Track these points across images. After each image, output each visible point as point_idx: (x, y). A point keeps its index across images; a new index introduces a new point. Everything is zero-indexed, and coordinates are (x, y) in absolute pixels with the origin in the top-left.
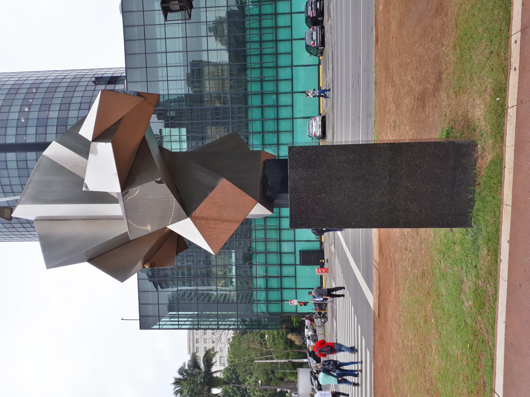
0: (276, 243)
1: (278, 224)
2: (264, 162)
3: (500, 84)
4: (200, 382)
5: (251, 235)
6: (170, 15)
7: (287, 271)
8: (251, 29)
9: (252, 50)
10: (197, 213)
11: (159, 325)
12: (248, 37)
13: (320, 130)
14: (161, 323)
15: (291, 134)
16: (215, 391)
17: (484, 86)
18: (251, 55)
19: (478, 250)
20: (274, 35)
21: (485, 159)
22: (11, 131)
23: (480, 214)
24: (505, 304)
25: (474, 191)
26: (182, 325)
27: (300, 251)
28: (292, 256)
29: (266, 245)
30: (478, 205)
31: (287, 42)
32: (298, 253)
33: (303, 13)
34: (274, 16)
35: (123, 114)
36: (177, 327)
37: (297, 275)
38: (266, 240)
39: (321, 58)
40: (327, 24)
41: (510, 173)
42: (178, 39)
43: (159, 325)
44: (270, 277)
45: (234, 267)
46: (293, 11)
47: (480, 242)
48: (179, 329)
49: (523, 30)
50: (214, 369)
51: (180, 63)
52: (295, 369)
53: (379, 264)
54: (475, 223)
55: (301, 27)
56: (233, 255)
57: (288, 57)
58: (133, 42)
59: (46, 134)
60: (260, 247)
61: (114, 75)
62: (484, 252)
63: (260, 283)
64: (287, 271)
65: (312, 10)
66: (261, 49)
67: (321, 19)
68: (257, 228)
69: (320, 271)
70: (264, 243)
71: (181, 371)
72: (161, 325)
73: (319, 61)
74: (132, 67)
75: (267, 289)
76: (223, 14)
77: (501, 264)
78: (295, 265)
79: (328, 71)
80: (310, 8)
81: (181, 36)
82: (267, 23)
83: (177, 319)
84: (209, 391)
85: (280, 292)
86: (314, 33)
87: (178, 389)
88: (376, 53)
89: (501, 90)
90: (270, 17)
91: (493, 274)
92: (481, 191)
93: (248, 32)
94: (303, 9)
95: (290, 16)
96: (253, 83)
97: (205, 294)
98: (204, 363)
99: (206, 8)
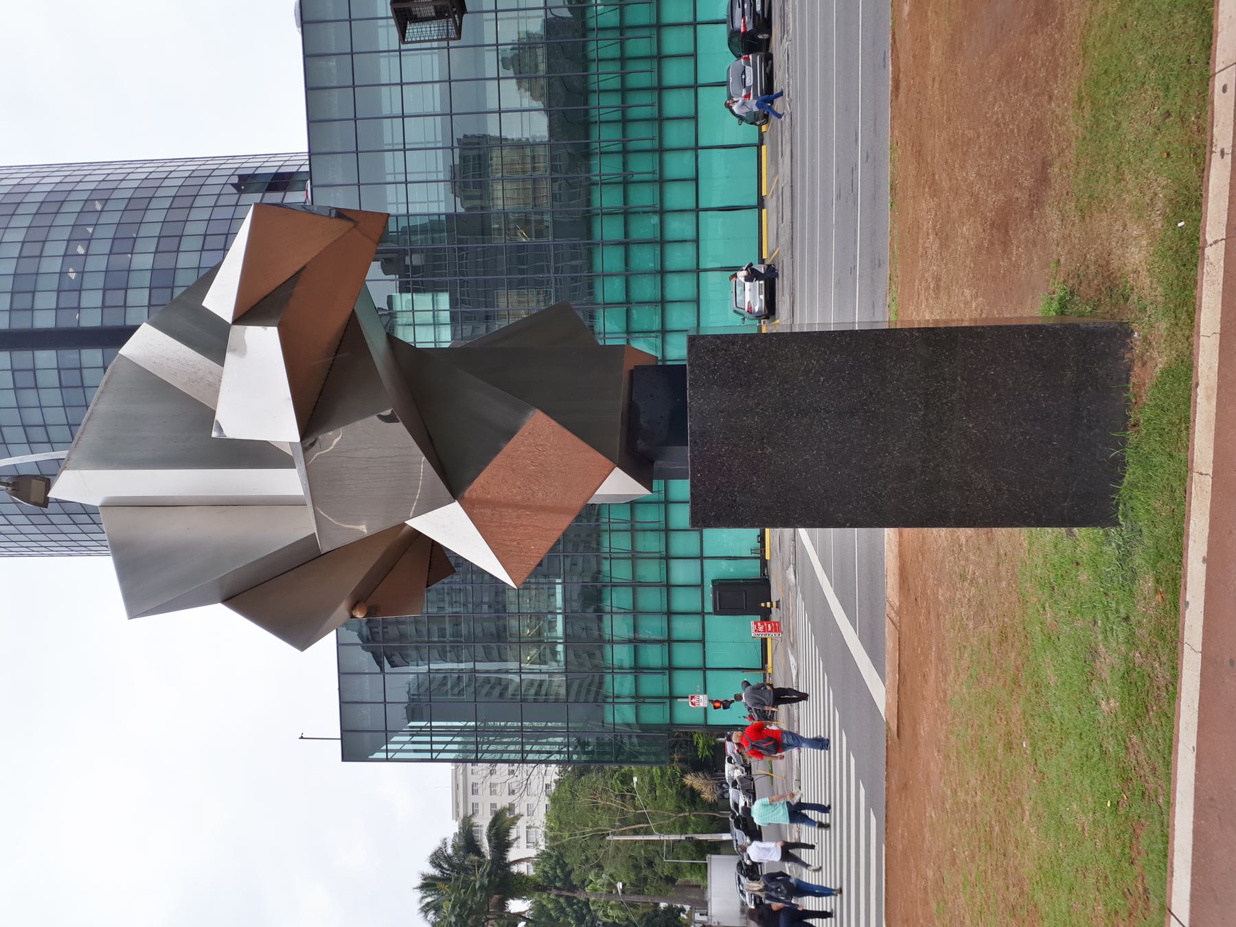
1: (662, 518)
4: (482, 886)
5: (599, 543)
6: (413, 30)
7: (684, 627)
8: (600, 60)
9: (602, 111)
11: (387, 751)
13: (762, 297)
14: (390, 747)
15: (693, 307)
16: (517, 906)
17: (1149, 194)
18: (601, 122)
19: (1133, 581)
20: (655, 40)
21: (1150, 365)
23: (1138, 497)
26: (439, 751)
27: (713, 581)
32: (709, 587)
34: (654, 31)
36: (428, 756)
37: (708, 637)
38: (634, 556)
39: (764, 128)
40: (779, 49)
42: (430, 86)
43: (387, 751)
44: (645, 641)
47: (1138, 560)
48: (432, 760)
50: (512, 855)
51: (436, 142)
52: (702, 855)
54: (1125, 516)
55: (718, 58)
56: (559, 589)
57: (688, 126)
58: (326, 93)
60: (621, 571)
61: (282, 170)
62: (1146, 584)
63: (621, 655)
64: (684, 627)
65: (743, 16)
66: (624, 108)
67: (766, 36)
68: (614, 526)
69: (761, 628)
71: (437, 858)
72: (392, 751)
73: (761, 135)
74: (324, 150)
75: (638, 669)
76: (535, 25)
78: (702, 613)
79: (780, 160)
82: (640, 46)
83: (428, 739)
84: (502, 905)
85: (666, 677)
86: (749, 70)
87: (429, 899)
88: (893, 118)
90: (645, 32)
93: (593, 68)
94: (723, 14)
95: (692, 92)
97: (493, 681)
98: (490, 841)
99: (496, 11)
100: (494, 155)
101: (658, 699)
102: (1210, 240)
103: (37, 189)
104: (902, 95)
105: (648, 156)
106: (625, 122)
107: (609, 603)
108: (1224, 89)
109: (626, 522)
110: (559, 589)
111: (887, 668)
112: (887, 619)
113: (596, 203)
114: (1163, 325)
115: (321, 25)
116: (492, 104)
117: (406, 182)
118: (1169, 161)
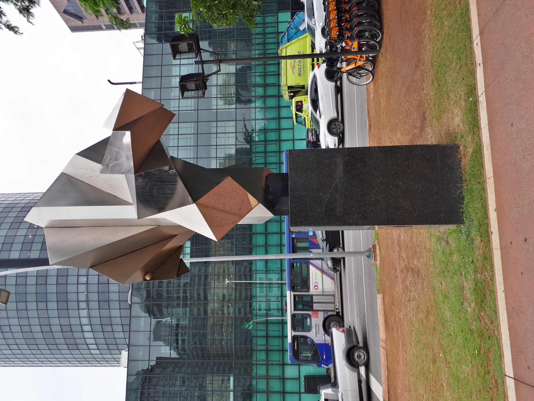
0: (279, 380)
1: (277, 70)
2: (267, 177)
3: (471, 86)
5: (251, 371)
6: (186, 94)
8: (256, 152)
10: (203, 200)
12: (254, 159)
15: (298, 381)
17: (458, 96)
18: (257, 233)
19: (473, 243)
20: (278, 157)
21: (467, 150)
22: (17, 247)
23: (470, 208)
24: (501, 272)
25: (462, 187)
27: (305, 377)
28: (296, 383)
29: (267, 355)
30: (467, 198)
31: (290, 142)
32: (302, 379)
33: (304, 139)
35: (144, 114)
38: (268, 378)
41: (488, 149)
45: (232, 393)
46: (295, 138)
47: (474, 233)
49: (481, 33)
53: (386, 342)
54: (466, 218)
56: (232, 378)
59: (46, 284)
60: (262, 385)
62: (477, 241)
65: (312, 135)
68: (258, 362)
70: (265, 366)
76: (233, 152)
77: (493, 236)
78: (300, 393)
80: (310, 134)
81: (192, 145)
85: (278, 133)
88: (369, 140)
89: (472, 90)
91: (488, 258)
92: (468, 187)
93: (254, 155)
94: (304, 137)
96: (258, 394)
99: (217, 133)
100: (208, 378)
101: (273, 85)
102: (480, 95)
103: (18, 206)
104: (372, 128)
105: (277, 353)
106: (267, 337)
107: (255, 372)
108: (480, 64)
109: (264, 360)
110: (232, 378)
111: (383, 380)
112: (381, 348)
113: (254, 243)
114: (470, 138)
115: (134, 362)
116: (214, 130)
117: (178, 135)
118: (464, 81)
